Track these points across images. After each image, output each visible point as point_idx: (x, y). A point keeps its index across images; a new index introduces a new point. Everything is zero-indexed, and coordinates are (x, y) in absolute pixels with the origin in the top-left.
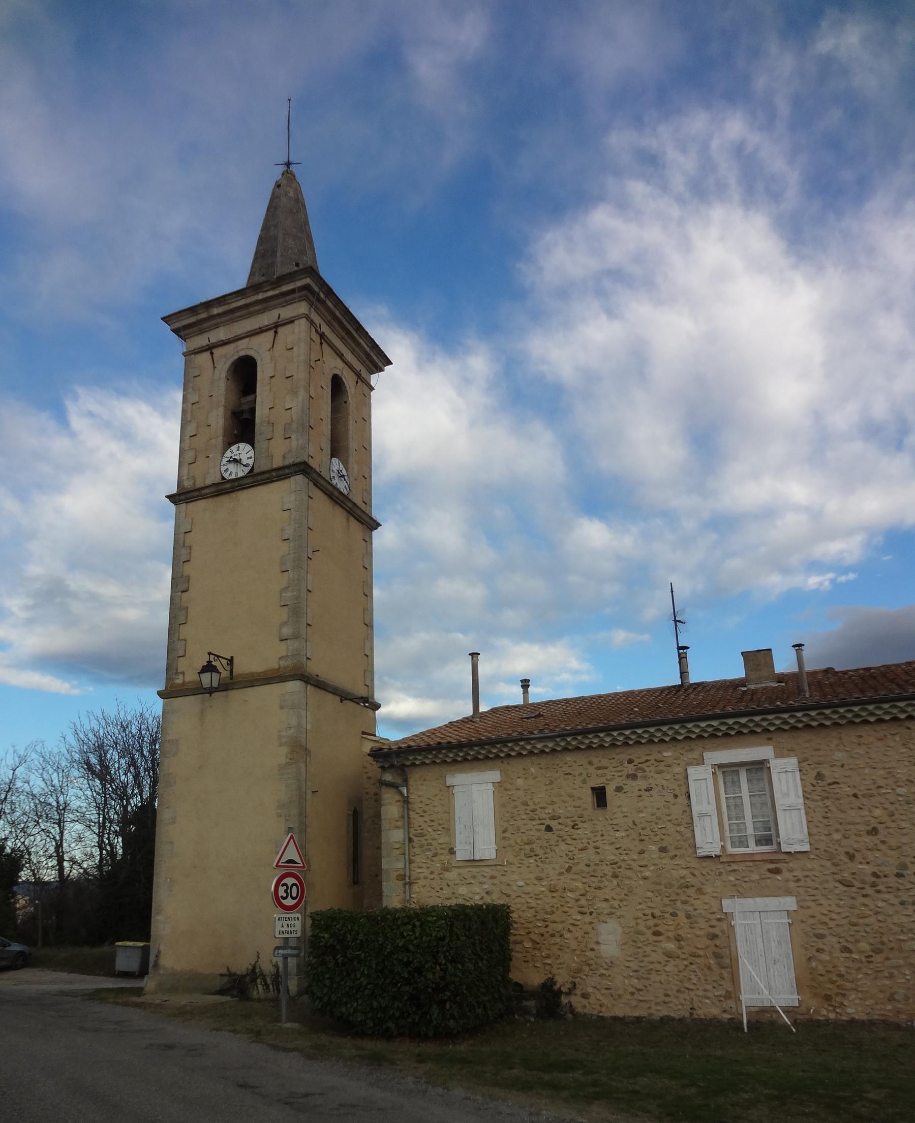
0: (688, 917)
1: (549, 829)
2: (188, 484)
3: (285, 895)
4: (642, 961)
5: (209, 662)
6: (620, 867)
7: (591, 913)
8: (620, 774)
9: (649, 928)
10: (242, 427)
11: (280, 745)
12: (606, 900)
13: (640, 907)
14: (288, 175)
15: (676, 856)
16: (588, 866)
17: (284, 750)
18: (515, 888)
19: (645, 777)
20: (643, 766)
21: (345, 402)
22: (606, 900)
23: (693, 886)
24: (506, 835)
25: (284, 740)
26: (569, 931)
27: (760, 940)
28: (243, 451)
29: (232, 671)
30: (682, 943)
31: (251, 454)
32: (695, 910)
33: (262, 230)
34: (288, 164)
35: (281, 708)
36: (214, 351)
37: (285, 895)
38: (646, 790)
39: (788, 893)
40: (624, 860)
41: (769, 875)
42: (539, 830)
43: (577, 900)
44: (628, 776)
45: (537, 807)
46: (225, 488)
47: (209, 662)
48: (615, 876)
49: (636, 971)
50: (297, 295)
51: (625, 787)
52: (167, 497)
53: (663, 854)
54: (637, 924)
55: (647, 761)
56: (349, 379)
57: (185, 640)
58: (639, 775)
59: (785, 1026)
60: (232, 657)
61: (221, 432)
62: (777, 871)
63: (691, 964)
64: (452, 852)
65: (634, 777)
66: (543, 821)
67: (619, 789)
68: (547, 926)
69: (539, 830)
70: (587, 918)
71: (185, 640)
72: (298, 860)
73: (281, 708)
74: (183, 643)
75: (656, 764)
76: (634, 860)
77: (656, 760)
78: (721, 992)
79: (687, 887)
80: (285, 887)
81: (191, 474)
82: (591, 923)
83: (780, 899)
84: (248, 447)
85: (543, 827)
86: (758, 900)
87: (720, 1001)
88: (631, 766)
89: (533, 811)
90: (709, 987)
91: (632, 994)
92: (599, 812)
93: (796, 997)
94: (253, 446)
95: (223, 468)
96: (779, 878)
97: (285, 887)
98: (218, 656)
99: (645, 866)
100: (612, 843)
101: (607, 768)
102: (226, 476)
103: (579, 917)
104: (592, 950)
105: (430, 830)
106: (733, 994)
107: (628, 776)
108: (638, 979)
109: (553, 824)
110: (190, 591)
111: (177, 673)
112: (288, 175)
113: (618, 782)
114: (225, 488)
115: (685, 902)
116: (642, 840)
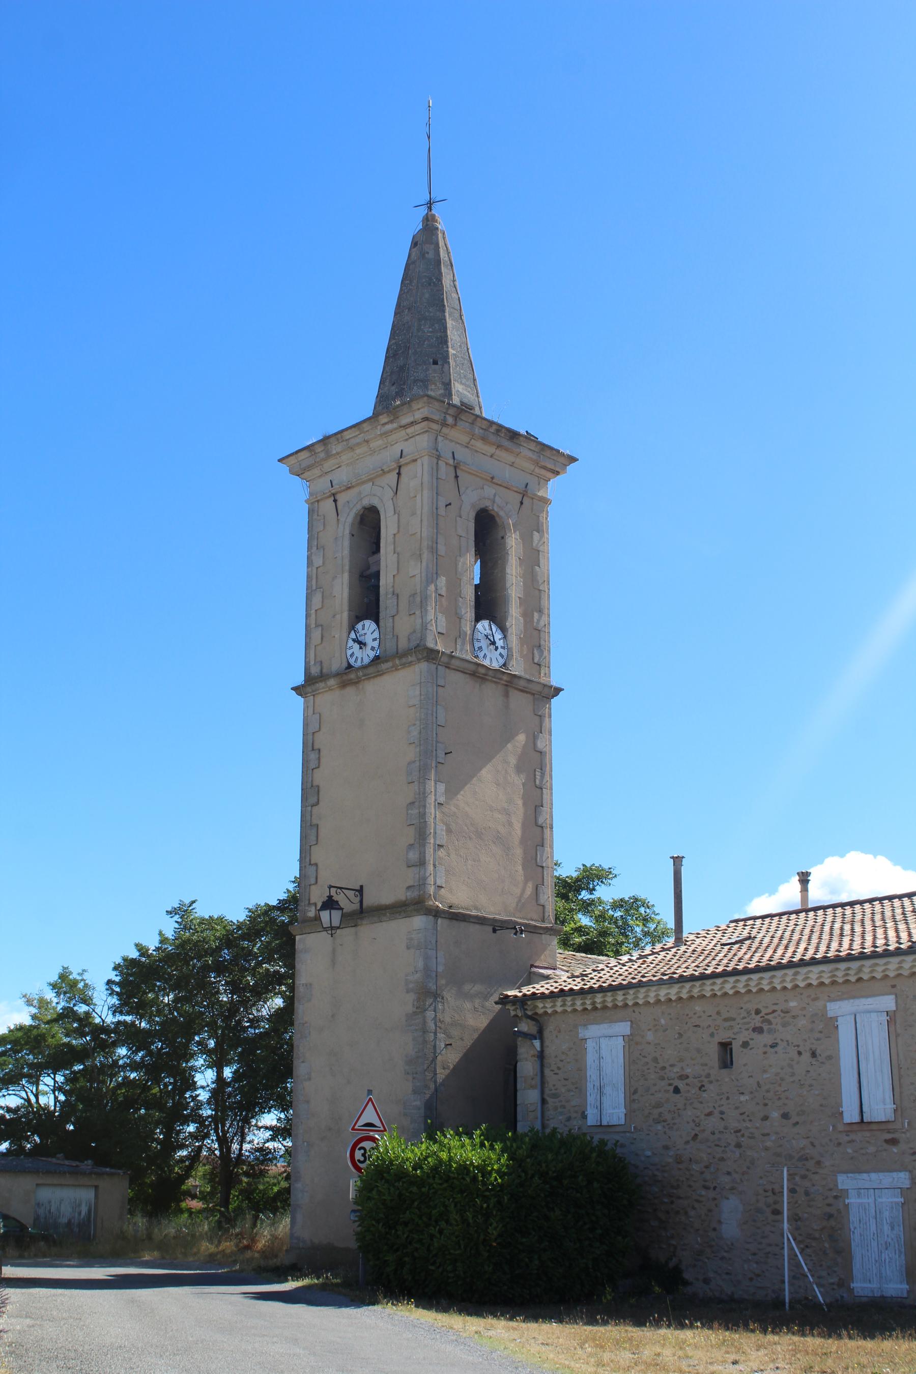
0: (807, 1193)
1: (677, 1090)
2: (315, 671)
3: (362, 1159)
4: (760, 1243)
5: (330, 897)
6: (743, 1136)
7: (715, 1188)
8: (747, 1026)
9: (768, 1206)
10: (368, 603)
11: (408, 992)
12: (729, 1173)
13: (761, 1182)
14: (429, 227)
15: (797, 1123)
16: (713, 1133)
17: (411, 997)
18: (643, 1159)
19: (770, 1031)
20: (770, 1017)
21: (503, 538)
22: (729, 1173)
23: (812, 1158)
24: (636, 1097)
25: (411, 986)
26: (694, 1208)
27: (873, 1221)
28: (368, 628)
29: (361, 902)
30: (799, 1223)
31: (376, 634)
32: (814, 1185)
33: (396, 314)
34: (430, 205)
35: (408, 948)
36: (338, 497)
37: (362, 1159)
38: (772, 1047)
39: (903, 1168)
40: (747, 1128)
41: (886, 1146)
42: (667, 1091)
43: (702, 1173)
44: (754, 1030)
45: (667, 1065)
46: (349, 676)
47: (330, 897)
48: (738, 1146)
49: (754, 1254)
50: (417, 428)
51: (751, 1042)
52: (292, 689)
53: (784, 1121)
54: (758, 1201)
55: (774, 1011)
56: (504, 506)
57: (316, 865)
58: (765, 1027)
59: (821, 1304)
60: (362, 887)
61: (346, 607)
62: (893, 1142)
63: (807, 1247)
64: (584, 1117)
65: (758, 1030)
66: (671, 1082)
67: (745, 1045)
68: (672, 1202)
69: (667, 1091)
70: (711, 1194)
71: (316, 865)
72: (377, 1122)
73: (408, 948)
74: (314, 868)
75: (783, 1015)
76: (757, 1128)
77: (782, 1011)
78: (834, 1280)
79: (807, 1159)
80: (362, 1151)
81: (318, 659)
82: (715, 1199)
83: (895, 1174)
84: (373, 626)
85: (671, 1088)
86: (874, 1176)
87: (833, 1289)
88: (758, 1018)
89: (664, 1068)
90: (824, 1273)
91: (751, 1279)
92: (724, 1071)
93: (905, 1286)
94: (377, 622)
95: (349, 652)
96: (895, 1150)
97: (362, 1151)
98: (341, 888)
99: (768, 1134)
100: (737, 1108)
101: (734, 1019)
102: (352, 661)
103: (703, 1193)
104: (715, 1229)
105: (563, 1090)
106: (844, 1283)
107: (754, 1030)
108: (757, 1263)
109: (681, 1085)
110: (321, 803)
111: (309, 903)
112: (429, 227)
113: (741, 1038)
114: (349, 676)
115: (804, 1177)
116: (766, 1105)
